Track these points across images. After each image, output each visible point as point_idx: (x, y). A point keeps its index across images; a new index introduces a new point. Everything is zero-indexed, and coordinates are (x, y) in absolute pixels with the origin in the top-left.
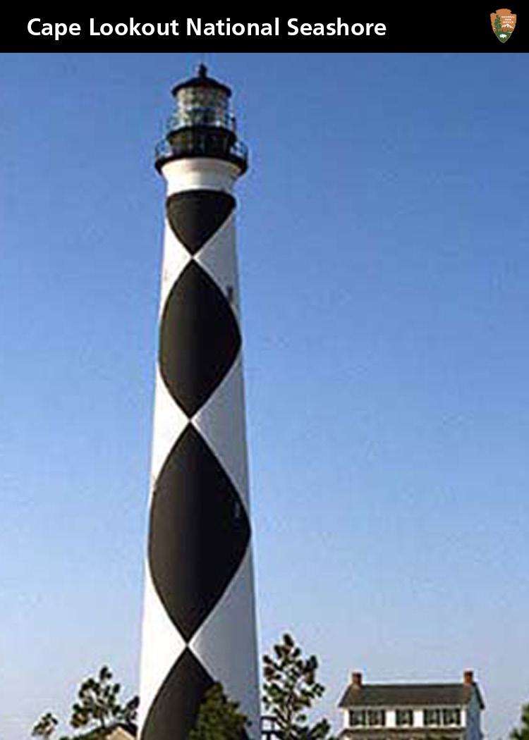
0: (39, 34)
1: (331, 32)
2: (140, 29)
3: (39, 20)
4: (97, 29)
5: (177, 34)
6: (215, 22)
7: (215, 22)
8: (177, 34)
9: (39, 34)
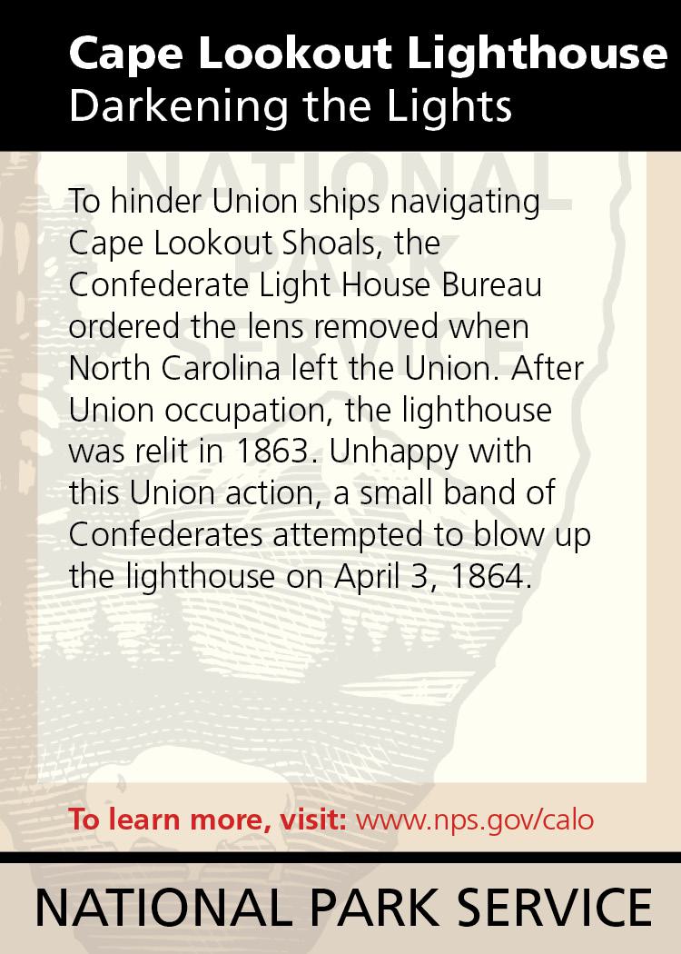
0: (93, 65)
1: (628, 62)
2: (309, 56)
3: (94, 39)
4: (216, 54)
5: (389, 66)
6: (506, 43)
7: (506, 43)
8: (389, 66)
9: (93, 65)
